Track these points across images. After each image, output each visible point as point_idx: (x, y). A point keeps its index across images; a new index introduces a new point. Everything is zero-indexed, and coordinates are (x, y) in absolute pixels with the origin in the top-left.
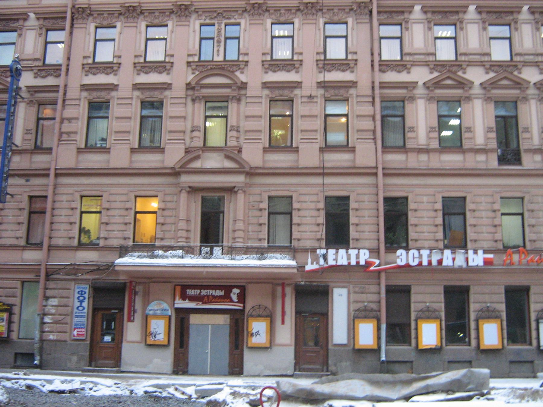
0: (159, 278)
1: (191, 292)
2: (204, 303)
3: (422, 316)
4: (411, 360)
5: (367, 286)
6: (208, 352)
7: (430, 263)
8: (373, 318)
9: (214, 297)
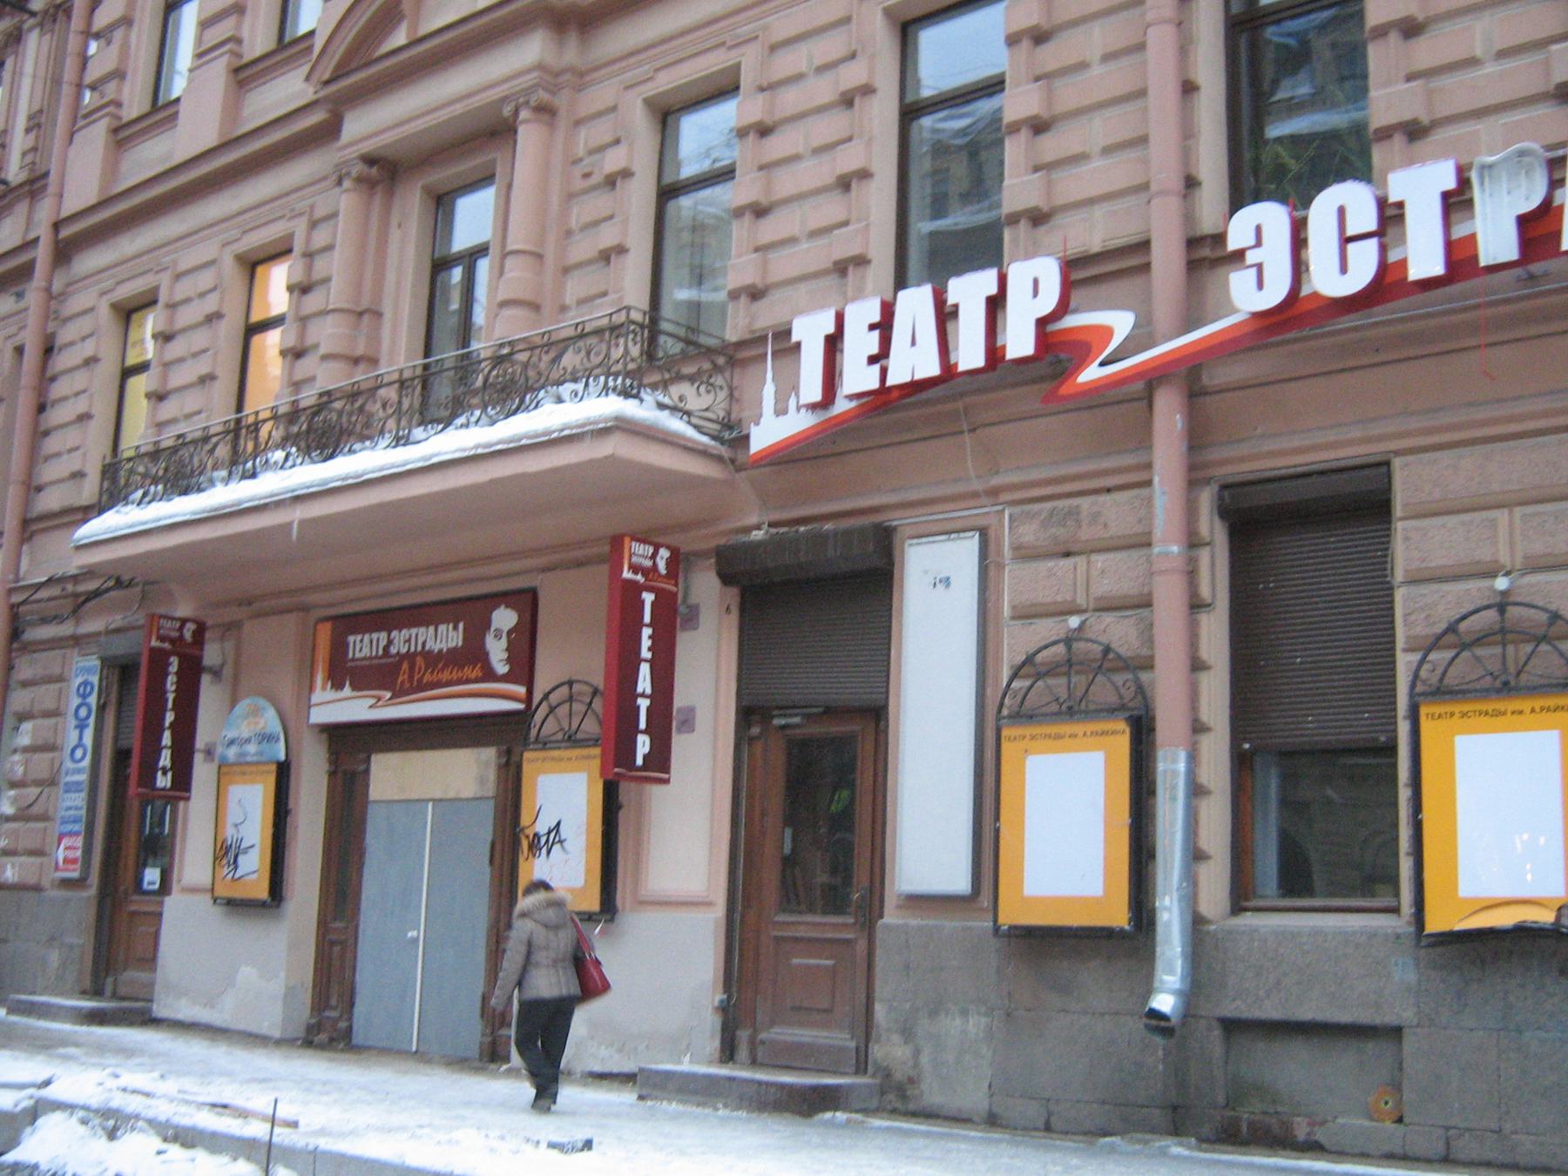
0: (280, 594)
1: (363, 646)
2: (399, 693)
3: (1452, 679)
4: (1388, 1018)
5: (1085, 503)
6: (415, 940)
7: (1460, 257)
8: (1112, 711)
9: (434, 660)
